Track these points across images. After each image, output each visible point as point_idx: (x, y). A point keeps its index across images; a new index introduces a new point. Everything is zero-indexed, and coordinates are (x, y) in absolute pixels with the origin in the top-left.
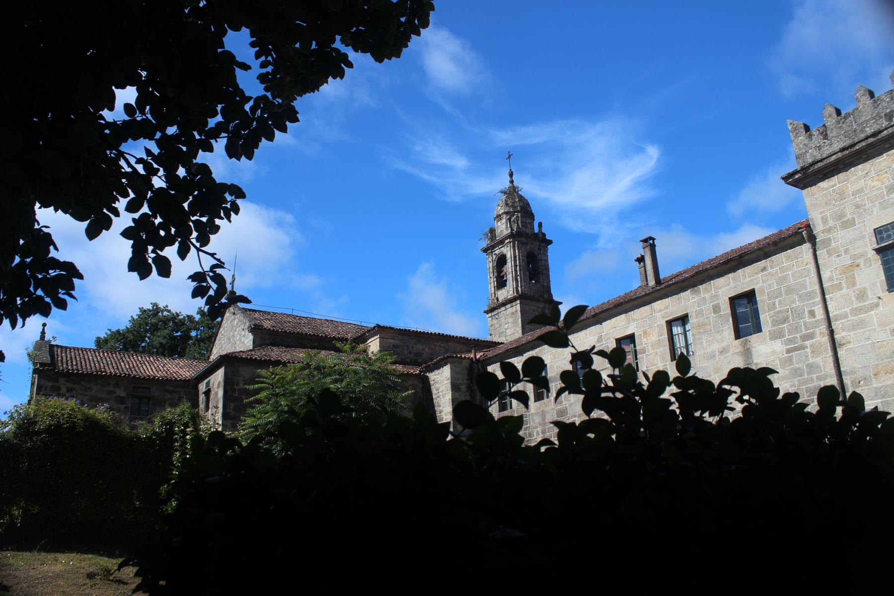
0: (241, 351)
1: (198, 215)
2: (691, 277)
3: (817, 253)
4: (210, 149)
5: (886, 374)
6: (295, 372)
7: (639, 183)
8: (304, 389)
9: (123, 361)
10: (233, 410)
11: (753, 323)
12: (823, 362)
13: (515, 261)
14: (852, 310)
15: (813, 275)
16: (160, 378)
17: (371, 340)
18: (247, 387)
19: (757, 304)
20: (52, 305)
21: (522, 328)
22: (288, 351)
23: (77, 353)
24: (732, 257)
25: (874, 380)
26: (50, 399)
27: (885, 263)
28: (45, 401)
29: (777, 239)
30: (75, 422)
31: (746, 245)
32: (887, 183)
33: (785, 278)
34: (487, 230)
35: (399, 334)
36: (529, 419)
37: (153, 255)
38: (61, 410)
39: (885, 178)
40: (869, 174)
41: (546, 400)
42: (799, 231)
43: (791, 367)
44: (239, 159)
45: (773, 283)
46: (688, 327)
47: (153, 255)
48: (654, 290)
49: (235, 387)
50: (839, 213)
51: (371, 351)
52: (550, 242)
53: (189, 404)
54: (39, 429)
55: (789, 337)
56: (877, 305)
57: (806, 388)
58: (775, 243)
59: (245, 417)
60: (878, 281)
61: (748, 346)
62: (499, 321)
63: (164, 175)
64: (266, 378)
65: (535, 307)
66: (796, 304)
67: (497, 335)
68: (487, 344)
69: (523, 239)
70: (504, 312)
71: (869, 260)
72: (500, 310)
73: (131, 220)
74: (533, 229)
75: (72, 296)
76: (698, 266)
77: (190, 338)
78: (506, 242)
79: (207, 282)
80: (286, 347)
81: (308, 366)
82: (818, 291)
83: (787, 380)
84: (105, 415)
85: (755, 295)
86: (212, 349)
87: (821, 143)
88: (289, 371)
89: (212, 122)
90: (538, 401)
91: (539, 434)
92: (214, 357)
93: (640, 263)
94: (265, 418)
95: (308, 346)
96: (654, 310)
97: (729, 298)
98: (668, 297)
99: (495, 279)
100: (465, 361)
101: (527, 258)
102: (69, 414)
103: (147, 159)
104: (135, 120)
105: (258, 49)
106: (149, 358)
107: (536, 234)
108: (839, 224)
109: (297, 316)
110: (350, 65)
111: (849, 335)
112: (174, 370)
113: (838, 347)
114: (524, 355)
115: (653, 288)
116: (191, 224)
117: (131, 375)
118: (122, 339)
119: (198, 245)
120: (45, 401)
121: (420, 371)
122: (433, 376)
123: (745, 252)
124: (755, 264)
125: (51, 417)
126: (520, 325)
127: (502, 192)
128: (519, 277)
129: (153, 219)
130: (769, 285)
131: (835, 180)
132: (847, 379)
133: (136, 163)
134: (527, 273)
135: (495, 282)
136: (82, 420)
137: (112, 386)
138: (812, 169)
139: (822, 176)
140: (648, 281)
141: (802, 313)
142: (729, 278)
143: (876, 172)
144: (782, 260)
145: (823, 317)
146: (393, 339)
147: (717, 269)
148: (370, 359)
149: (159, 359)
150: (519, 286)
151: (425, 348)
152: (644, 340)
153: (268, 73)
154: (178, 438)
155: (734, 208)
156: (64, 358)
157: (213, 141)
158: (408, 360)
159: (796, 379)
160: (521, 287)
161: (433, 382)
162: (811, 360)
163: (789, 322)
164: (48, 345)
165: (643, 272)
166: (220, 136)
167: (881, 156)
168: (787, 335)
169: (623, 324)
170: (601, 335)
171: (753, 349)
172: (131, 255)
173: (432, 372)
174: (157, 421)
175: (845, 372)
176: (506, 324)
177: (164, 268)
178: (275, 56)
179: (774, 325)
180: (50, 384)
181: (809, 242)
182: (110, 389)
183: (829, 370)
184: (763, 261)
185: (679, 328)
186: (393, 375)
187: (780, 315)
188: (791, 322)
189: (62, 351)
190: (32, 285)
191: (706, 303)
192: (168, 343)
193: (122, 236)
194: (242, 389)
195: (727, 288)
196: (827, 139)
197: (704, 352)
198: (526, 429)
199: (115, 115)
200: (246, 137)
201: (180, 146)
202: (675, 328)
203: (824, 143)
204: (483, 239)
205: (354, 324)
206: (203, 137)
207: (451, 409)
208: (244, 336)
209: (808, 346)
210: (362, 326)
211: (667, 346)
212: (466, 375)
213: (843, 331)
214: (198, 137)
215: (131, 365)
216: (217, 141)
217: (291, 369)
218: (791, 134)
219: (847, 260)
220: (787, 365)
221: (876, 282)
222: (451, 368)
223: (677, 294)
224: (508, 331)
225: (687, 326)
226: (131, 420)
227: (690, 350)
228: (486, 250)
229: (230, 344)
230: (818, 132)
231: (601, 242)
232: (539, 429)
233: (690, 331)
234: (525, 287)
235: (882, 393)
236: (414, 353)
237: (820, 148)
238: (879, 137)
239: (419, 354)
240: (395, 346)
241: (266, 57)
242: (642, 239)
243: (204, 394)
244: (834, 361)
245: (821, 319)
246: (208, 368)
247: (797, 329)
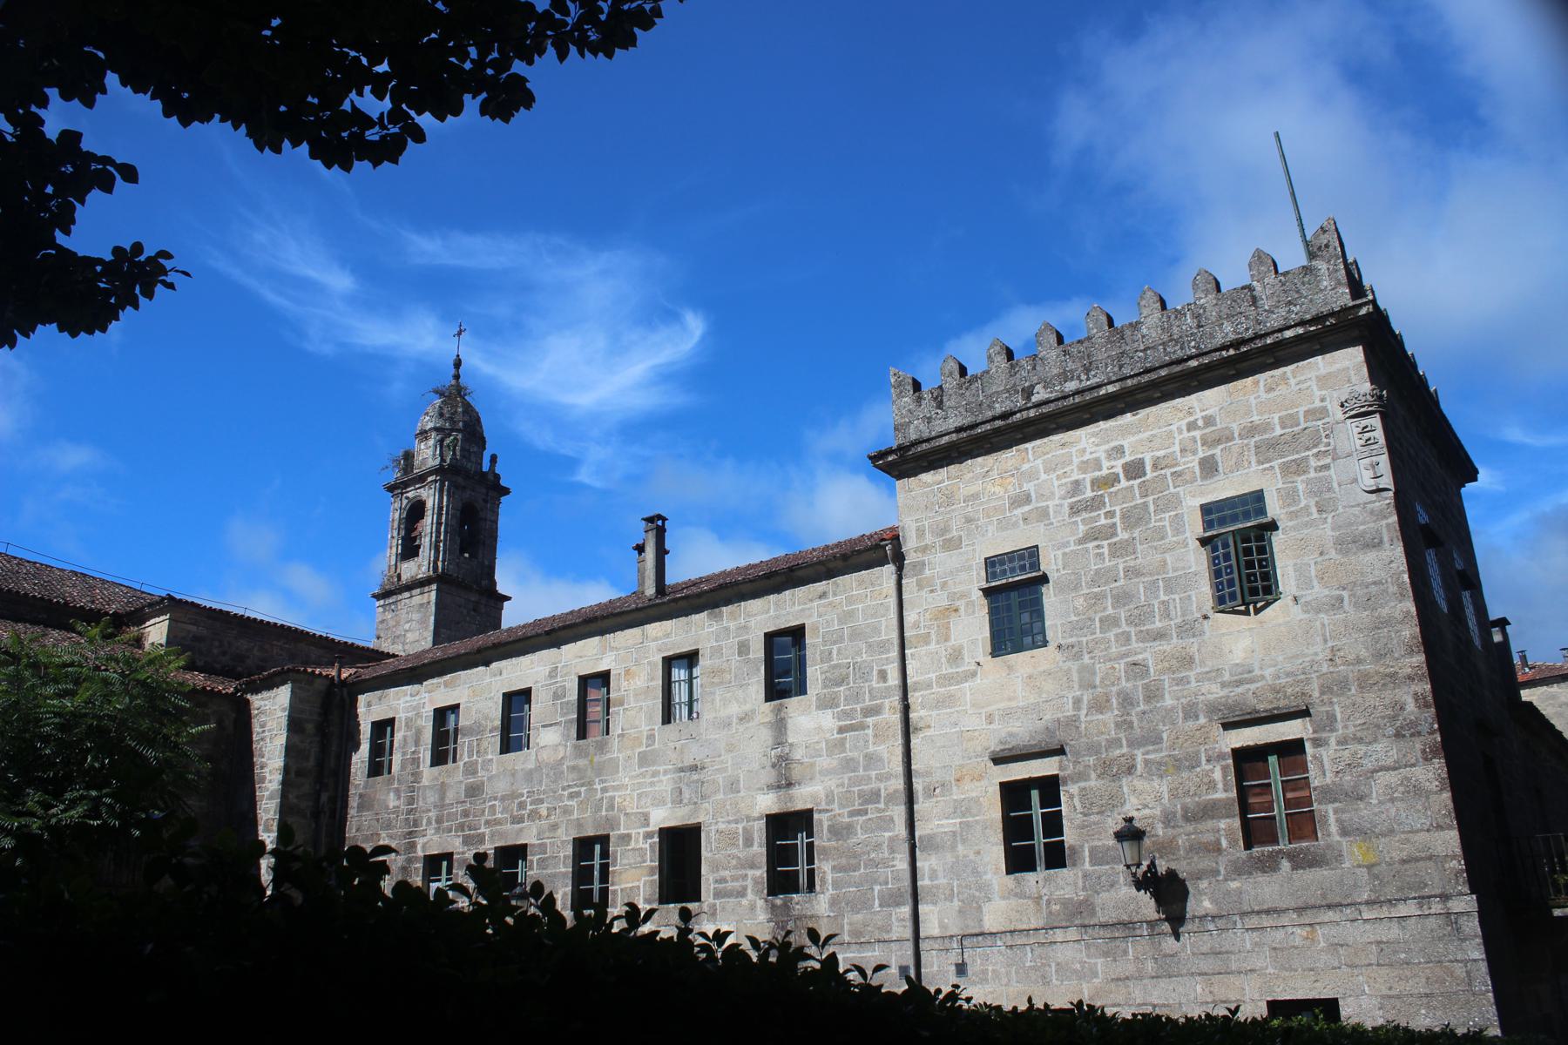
2: (711, 591)
3: (903, 582)
5: (972, 780)
11: (796, 678)
13: (440, 515)
14: (939, 678)
17: (152, 621)
25: (954, 788)
27: (993, 613)
32: (1012, 492)
33: (850, 615)
34: (401, 453)
36: (418, 796)
39: (1010, 484)
40: (990, 473)
41: (450, 765)
43: (842, 755)
45: (833, 620)
46: (696, 672)
48: (651, 603)
50: (942, 526)
52: (506, 491)
55: (846, 708)
56: (974, 674)
57: (859, 790)
58: (845, 557)
60: (980, 638)
61: (782, 715)
67: (389, 640)
69: (460, 480)
70: (407, 601)
71: (973, 602)
72: (400, 597)
74: (481, 464)
76: (730, 573)
78: (430, 479)
82: (896, 642)
83: (833, 776)
90: (437, 765)
91: (431, 823)
98: (672, 619)
99: (400, 542)
100: (318, 681)
107: (484, 474)
109: (15, 558)
111: (931, 716)
113: (913, 732)
114: (425, 683)
115: (650, 600)
122: (257, 701)
123: (798, 564)
126: (432, 628)
127: (436, 392)
128: (441, 545)
131: (943, 473)
135: (400, 547)
143: (999, 472)
145: (897, 682)
146: (194, 624)
147: (754, 584)
150: (441, 559)
152: (624, 684)
158: (218, 666)
159: (846, 776)
160: (444, 561)
161: (256, 712)
162: (871, 749)
167: (1009, 450)
169: (594, 653)
170: (557, 667)
171: (789, 721)
173: (257, 694)
175: (916, 771)
176: (408, 622)
179: (825, 687)
181: (894, 563)
185: (682, 671)
186: (177, 692)
187: (837, 673)
188: (851, 685)
195: (763, 617)
197: (714, 715)
198: (411, 811)
203: (937, 413)
204: (390, 469)
205: (127, 587)
207: (282, 764)
210: (143, 592)
211: (658, 698)
213: (923, 707)
219: (941, 600)
220: (836, 751)
221: (977, 639)
222: (292, 691)
223: (687, 616)
224: (409, 635)
225: (694, 670)
227: (695, 710)
228: (394, 488)
230: (930, 395)
232: (432, 814)
233: (699, 679)
235: (963, 809)
237: (929, 420)
238: (1010, 421)
240: (196, 638)
242: (645, 517)
247: (856, 697)
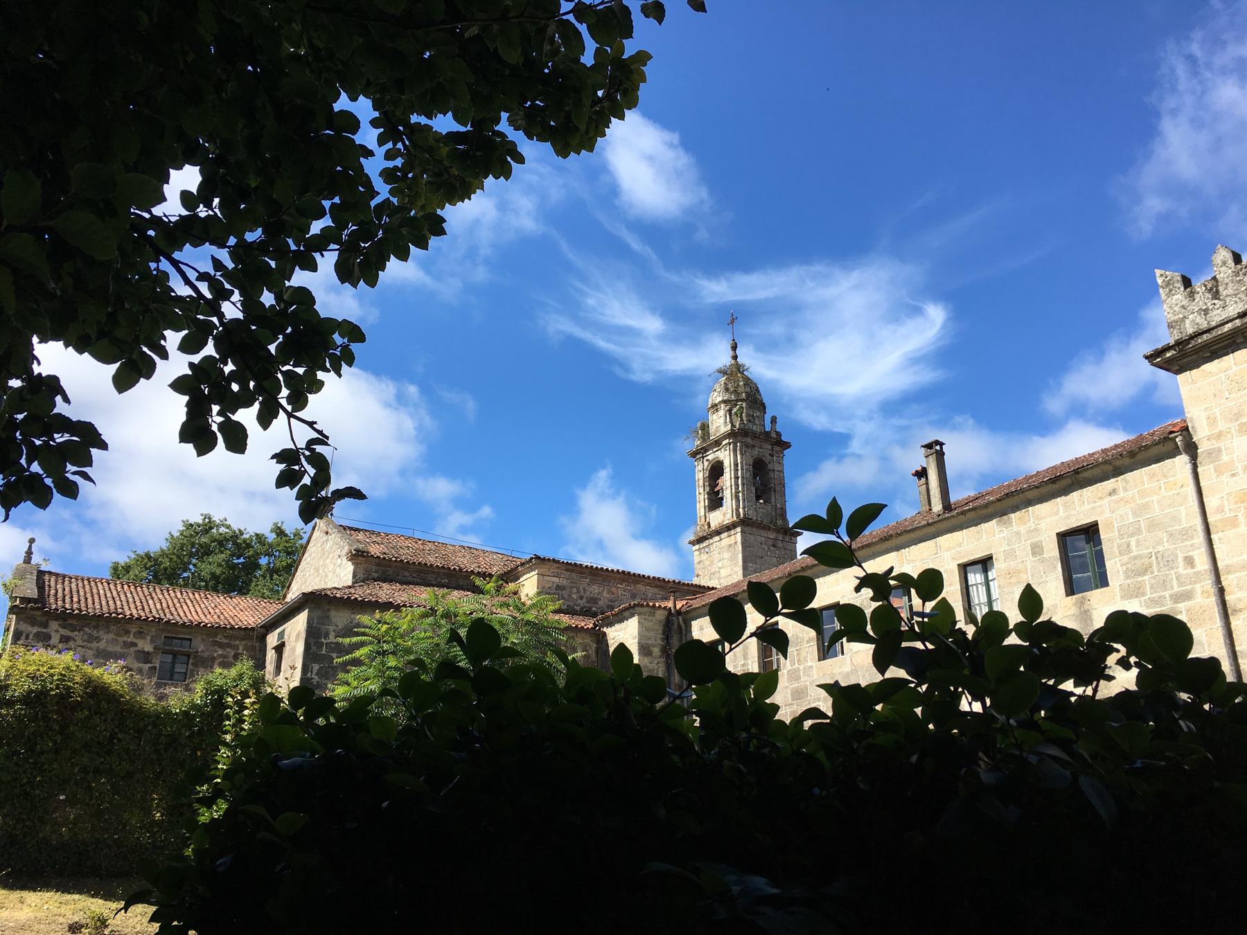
0: (334, 588)
1: (291, 363)
2: (998, 500)
3: (1199, 470)
4: (313, 267)
6: (413, 620)
7: (915, 360)
8: (425, 645)
9: (152, 598)
10: (317, 674)
11: (1094, 572)
12: (1207, 635)
15: (1191, 504)
16: (208, 625)
17: (525, 577)
18: (340, 640)
19: (1101, 544)
20: (54, 490)
21: (743, 569)
22: (404, 590)
23: (80, 584)
24: (1062, 473)
26: (32, 652)
28: (25, 654)
29: (1135, 448)
30: (69, 688)
31: (1084, 456)
33: (1145, 507)
35: (567, 570)
37: (220, 419)
38: (49, 668)
42: (1170, 436)
44: (355, 285)
45: (1127, 514)
46: (991, 575)
47: (220, 419)
49: (323, 640)
51: (525, 593)
52: (787, 445)
53: (251, 663)
54: (12, 696)
55: (1153, 596)
58: (1132, 454)
59: (334, 684)
61: (1086, 607)
62: (710, 556)
63: (240, 301)
64: (370, 628)
65: (763, 538)
66: (1164, 547)
67: (707, 577)
68: (692, 589)
72: (711, 541)
73: (187, 365)
75: (86, 477)
77: (258, 566)
78: (724, 443)
79: (301, 464)
80: (401, 584)
81: (433, 611)
84: (119, 677)
85: (1098, 530)
86: (290, 585)
87: (1209, 304)
88: (404, 618)
89: (316, 227)
92: (293, 594)
93: (920, 479)
94: (364, 686)
95: (434, 583)
96: (940, 547)
97: (1057, 534)
99: (706, 496)
101: (753, 468)
102: (61, 675)
103: (215, 274)
104: (196, 215)
105: (382, 130)
106: (194, 594)
107: (767, 434)
108: (1234, 426)
109: (420, 540)
110: (520, 159)
112: (230, 613)
113: (1232, 614)
115: (939, 515)
116: (280, 376)
117: (163, 619)
118: (152, 566)
119: (289, 408)
120: (25, 654)
121: (594, 624)
123: (1083, 466)
124: (1099, 484)
125: (32, 678)
128: (740, 494)
129: (222, 366)
130: (1121, 516)
132: (1245, 664)
133: (197, 279)
134: (753, 490)
135: (706, 501)
136: (81, 684)
137: (132, 635)
138: (1193, 343)
139: (1208, 354)
140: (932, 505)
141: (1172, 561)
142: (1057, 504)
144: (1142, 478)
148: (524, 604)
149: (208, 596)
150: (741, 506)
151: (603, 591)
153: (396, 167)
154: (231, 714)
155: (1054, 405)
156: (60, 591)
157: (317, 256)
158: (578, 608)
160: (744, 508)
163: (1152, 573)
164: (35, 572)
165: (924, 493)
166: (328, 248)
168: (1148, 593)
171: (1094, 612)
172: (184, 418)
174: (199, 688)
176: (720, 561)
177: (237, 439)
178: (407, 143)
179: (1128, 577)
180: (35, 630)
181: (1187, 453)
182: (129, 640)
183: (1217, 648)
184: (1112, 480)
185: (978, 576)
186: (555, 628)
189: (56, 582)
190: (24, 456)
191: (1021, 541)
192: (224, 573)
193: (172, 388)
194: (333, 643)
196: (1219, 299)
199: (171, 208)
200: (367, 254)
201: (266, 259)
202: (973, 575)
203: (1214, 304)
205: (502, 554)
206: (302, 248)
208: (339, 565)
209: (1183, 610)
210: (513, 557)
212: (661, 632)
213: (1240, 589)
214: (293, 247)
215: (165, 605)
216: (323, 256)
217: (407, 615)
218: (1161, 290)
222: (639, 622)
223: (976, 525)
224: (722, 571)
225: (989, 573)
226: (158, 686)
229: (319, 578)
230: (1204, 288)
231: (855, 446)
234: (750, 509)
236: (587, 598)
237: (1206, 311)
239: (594, 600)
240: (558, 587)
241: (395, 144)
242: (924, 444)
243: (274, 650)
244: (1224, 636)
245: (1205, 570)
246: (282, 611)
247: (1164, 584)
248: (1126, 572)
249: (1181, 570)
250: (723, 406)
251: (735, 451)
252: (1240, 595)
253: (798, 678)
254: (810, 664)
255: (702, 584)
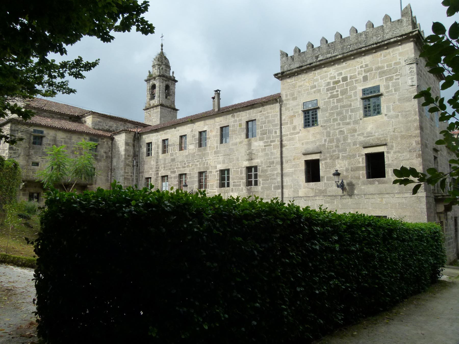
33: (268, 117)
45: (263, 118)
49: (16, 135)
52: (176, 81)
134: (165, 95)
179: (261, 135)
237: (290, 65)
239: (111, 127)
248: (261, 134)
249: (273, 135)
250: (157, 66)
251: (160, 81)
252: (285, 142)
253: (173, 156)
254: (177, 152)
255: (147, 124)
